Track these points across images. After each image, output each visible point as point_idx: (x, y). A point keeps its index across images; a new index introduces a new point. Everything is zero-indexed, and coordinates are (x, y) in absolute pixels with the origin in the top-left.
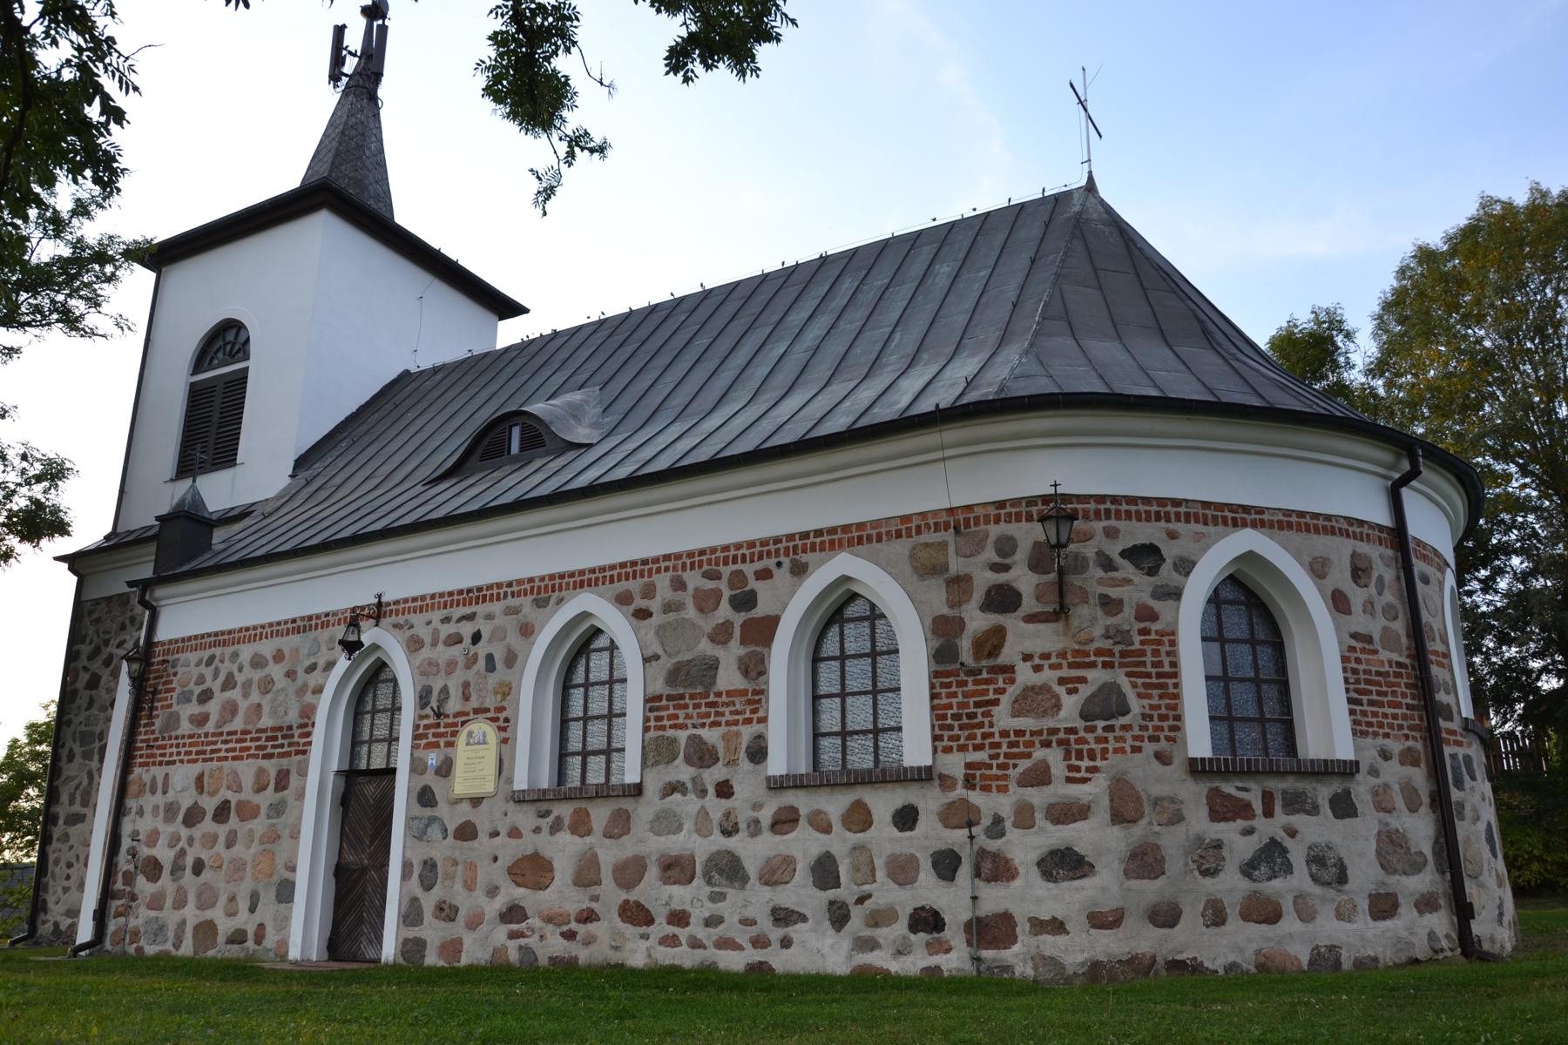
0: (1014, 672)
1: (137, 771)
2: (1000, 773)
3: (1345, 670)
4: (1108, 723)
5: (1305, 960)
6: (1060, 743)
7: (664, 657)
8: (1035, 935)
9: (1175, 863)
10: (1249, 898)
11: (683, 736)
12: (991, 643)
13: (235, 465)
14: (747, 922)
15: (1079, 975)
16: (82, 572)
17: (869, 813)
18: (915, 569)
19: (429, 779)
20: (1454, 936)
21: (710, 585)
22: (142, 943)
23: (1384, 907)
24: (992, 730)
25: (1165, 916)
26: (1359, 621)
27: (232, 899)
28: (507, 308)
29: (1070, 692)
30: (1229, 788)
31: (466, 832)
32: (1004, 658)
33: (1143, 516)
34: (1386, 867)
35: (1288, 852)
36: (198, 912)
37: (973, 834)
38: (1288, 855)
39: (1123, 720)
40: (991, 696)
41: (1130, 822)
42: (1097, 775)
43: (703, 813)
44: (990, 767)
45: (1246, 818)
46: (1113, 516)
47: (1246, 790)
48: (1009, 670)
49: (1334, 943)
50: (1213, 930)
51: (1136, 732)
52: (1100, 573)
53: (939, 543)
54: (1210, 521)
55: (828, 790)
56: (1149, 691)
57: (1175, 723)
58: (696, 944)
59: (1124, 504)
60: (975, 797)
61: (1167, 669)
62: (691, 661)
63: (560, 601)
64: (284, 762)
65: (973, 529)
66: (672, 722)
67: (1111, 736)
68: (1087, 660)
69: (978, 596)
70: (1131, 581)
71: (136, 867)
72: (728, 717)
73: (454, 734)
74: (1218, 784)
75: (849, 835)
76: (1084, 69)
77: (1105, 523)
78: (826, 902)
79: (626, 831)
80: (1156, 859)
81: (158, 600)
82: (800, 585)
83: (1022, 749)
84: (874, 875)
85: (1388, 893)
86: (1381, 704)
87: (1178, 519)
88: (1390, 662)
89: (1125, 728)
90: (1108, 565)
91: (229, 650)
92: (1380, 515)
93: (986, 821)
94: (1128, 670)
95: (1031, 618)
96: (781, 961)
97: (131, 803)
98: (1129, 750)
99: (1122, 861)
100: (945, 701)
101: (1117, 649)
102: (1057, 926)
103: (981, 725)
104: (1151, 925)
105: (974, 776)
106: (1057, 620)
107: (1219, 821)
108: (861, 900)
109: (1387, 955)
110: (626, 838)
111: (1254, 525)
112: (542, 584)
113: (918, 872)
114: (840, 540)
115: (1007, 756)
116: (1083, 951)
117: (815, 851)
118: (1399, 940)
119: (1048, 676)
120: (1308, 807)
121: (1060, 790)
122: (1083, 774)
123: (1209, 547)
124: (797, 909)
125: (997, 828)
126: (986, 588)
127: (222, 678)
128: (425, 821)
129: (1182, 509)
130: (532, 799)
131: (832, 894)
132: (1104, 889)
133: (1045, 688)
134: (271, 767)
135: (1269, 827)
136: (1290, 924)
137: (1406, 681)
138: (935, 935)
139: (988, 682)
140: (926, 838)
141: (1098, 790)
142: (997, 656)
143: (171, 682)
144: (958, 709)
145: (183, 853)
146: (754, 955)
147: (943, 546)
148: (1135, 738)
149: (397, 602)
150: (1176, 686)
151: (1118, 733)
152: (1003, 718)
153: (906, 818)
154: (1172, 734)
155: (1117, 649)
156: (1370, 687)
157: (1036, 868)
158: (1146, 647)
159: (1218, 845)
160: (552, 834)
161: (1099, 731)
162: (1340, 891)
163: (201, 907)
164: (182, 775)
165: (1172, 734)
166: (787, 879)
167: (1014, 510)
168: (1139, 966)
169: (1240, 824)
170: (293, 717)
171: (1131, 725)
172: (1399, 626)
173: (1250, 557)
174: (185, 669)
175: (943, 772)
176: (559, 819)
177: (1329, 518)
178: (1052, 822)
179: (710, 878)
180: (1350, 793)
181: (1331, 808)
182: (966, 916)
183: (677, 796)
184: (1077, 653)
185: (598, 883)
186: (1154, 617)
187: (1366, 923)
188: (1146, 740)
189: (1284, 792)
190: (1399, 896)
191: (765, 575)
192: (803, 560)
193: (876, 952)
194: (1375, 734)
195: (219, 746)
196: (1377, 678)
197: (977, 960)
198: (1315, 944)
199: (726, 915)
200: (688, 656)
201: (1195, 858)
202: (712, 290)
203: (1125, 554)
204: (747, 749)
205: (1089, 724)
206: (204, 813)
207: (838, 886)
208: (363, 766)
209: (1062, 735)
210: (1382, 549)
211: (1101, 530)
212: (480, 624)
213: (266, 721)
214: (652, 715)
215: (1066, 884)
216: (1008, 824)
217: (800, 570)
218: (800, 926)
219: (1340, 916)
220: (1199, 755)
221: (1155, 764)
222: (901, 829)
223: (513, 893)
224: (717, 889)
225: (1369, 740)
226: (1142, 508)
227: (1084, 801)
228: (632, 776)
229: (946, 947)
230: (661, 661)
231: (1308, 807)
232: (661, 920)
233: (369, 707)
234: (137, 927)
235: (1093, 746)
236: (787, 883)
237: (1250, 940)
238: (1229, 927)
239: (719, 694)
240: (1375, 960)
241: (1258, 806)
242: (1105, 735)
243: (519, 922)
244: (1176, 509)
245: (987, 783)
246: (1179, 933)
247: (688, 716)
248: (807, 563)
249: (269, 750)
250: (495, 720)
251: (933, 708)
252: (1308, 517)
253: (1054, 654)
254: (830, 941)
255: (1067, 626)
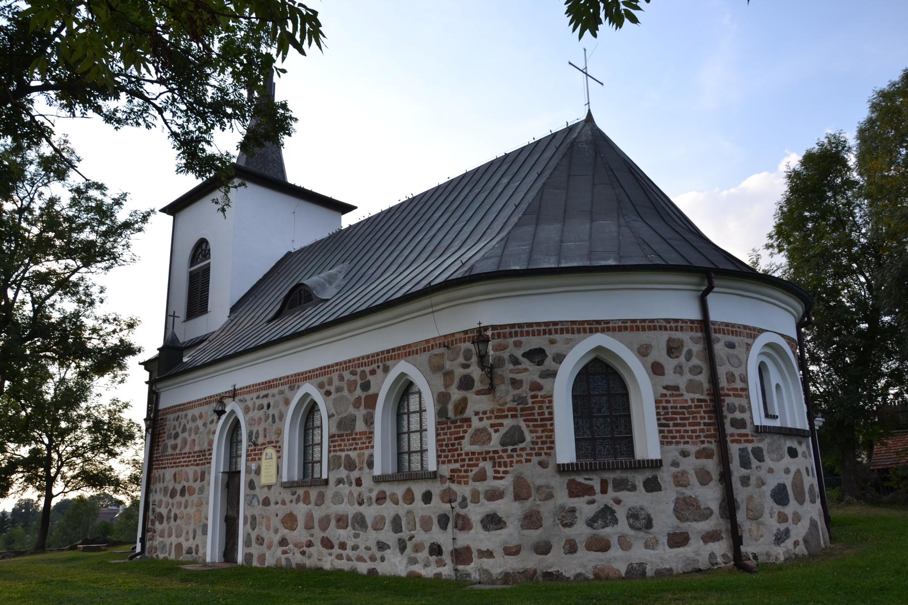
0: (471, 421)
1: (155, 471)
2: (465, 474)
3: (657, 408)
4: (514, 447)
5: (623, 571)
6: (492, 458)
7: (336, 415)
8: (480, 558)
9: (548, 521)
10: (591, 538)
11: (343, 454)
12: (462, 406)
13: (207, 312)
14: (367, 548)
15: (499, 580)
16: (152, 369)
17: (413, 494)
18: (431, 368)
19: (253, 476)
20: (730, 555)
21: (353, 378)
22: (158, 553)
23: (678, 540)
24: (462, 452)
25: (543, 549)
26: (670, 378)
27: (187, 533)
28: (346, 208)
29: (496, 431)
30: (580, 479)
31: (266, 502)
32: (466, 415)
33: (536, 333)
34: (680, 517)
35: (615, 512)
36: (176, 539)
37: (453, 506)
38: (615, 514)
39: (522, 445)
40: (461, 434)
41: (524, 499)
42: (507, 475)
43: (351, 493)
44: (460, 471)
45: (590, 495)
46: (519, 334)
47: (590, 479)
48: (468, 420)
49: (642, 561)
50: (569, 556)
51: (528, 451)
52: (511, 366)
53: (441, 354)
54: (576, 332)
55: (397, 483)
56: (536, 429)
57: (550, 445)
58: (349, 559)
59: (525, 327)
60: (455, 487)
61: (547, 416)
62: (346, 417)
63: (299, 387)
64: (203, 467)
65: (455, 346)
66: (339, 448)
67: (515, 454)
68: (503, 414)
69: (456, 381)
70: (528, 369)
71: (155, 517)
72: (360, 445)
73: (261, 454)
74: (573, 477)
75: (405, 505)
76: (585, 50)
77: (515, 339)
78: (397, 539)
79: (323, 503)
80: (537, 518)
81: (159, 389)
82: (386, 377)
83: (475, 462)
84: (415, 526)
85: (682, 533)
86: (685, 425)
87: (556, 332)
88: (692, 400)
89: (522, 449)
90: (515, 361)
91: (184, 413)
92: (692, 313)
93: (459, 500)
94: (525, 418)
95: (479, 393)
96: (383, 569)
97: (152, 487)
98: (524, 461)
99: (519, 520)
100: (442, 437)
101: (519, 407)
102: (489, 554)
103: (457, 450)
104: (535, 554)
105: (454, 476)
106: (489, 393)
107: (574, 497)
108: (411, 538)
109: (678, 567)
110: (323, 505)
111: (603, 331)
112: (292, 379)
113: (432, 525)
114: (402, 353)
115: (468, 466)
116: (501, 567)
117: (393, 514)
118: (688, 559)
119: (486, 423)
120: (629, 487)
121: (491, 483)
122: (501, 475)
123: (574, 346)
124: (386, 543)
125: (464, 504)
126: (460, 377)
127: (182, 427)
128: (252, 497)
129: (559, 327)
130: (289, 486)
131: (399, 535)
132: (511, 535)
133: (484, 430)
134: (199, 469)
135: (602, 500)
136: (615, 551)
137: (704, 409)
138: (439, 557)
139: (460, 427)
140: (435, 507)
141: (507, 483)
142: (463, 414)
143: (164, 429)
144: (448, 441)
145: (170, 511)
146: (369, 565)
147: (442, 355)
148: (528, 455)
149: (241, 389)
150: (552, 425)
151: (519, 452)
152: (467, 446)
153: (427, 497)
154: (548, 451)
155: (519, 407)
156: (675, 416)
157: (480, 524)
158: (535, 405)
159: (573, 510)
160: (297, 503)
161: (509, 452)
162: (648, 533)
163: (177, 537)
164: (169, 473)
165: (548, 451)
166: (382, 528)
167: (471, 335)
168: (529, 575)
169: (587, 498)
170: (206, 446)
171: (525, 448)
172: (703, 378)
173: (599, 348)
174: (169, 422)
175: (442, 474)
176: (299, 496)
177: (652, 321)
178: (487, 500)
179: (354, 526)
180: (657, 478)
181: (644, 486)
182: (451, 548)
183: (341, 485)
184: (499, 410)
185: (313, 528)
186: (539, 388)
187: (664, 550)
188: (534, 455)
189: (614, 480)
190: (690, 533)
191: (373, 372)
192: (388, 365)
193: (417, 565)
194: (678, 443)
195: (181, 460)
196: (681, 410)
197: (456, 570)
198: (630, 563)
199: (360, 545)
200: (345, 415)
201: (560, 518)
202: (557, 133)
203: (524, 355)
204: (367, 461)
205: (504, 448)
206: (177, 492)
207: (401, 531)
208: (234, 470)
209: (491, 454)
210: (693, 334)
211: (512, 343)
212: (271, 400)
213: (197, 448)
214: (332, 444)
215: (493, 532)
216: (469, 501)
217: (386, 370)
218: (388, 551)
219: (647, 546)
220: (566, 461)
221: (539, 469)
222: (425, 503)
223: (284, 532)
224: (356, 532)
225: (673, 446)
226: (535, 328)
227: (501, 489)
228: (324, 476)
229: (444, 563)
230: (335, 417)
231: (629, 487)
232: (336, 546)
233: (235, 440)
234: (156, 546)
235: (506, 460)
236: (382, 529)
237: (590, 561)
238: (578, 554)
239: (356, 434)
240: (671, 570)
241: (597, 488)
242: (512, 453)
243: (286, 546)
244: (555, 327)
245: (460, 479)
246: (550, 558)
247: (345, 445)
248: (389, 366)
249: (198, 462)
250: (275, 447)
251: (437, 441)
252: (638, 322)
253: (488, 411)
254: (399, 559)
255: (494, 396)
